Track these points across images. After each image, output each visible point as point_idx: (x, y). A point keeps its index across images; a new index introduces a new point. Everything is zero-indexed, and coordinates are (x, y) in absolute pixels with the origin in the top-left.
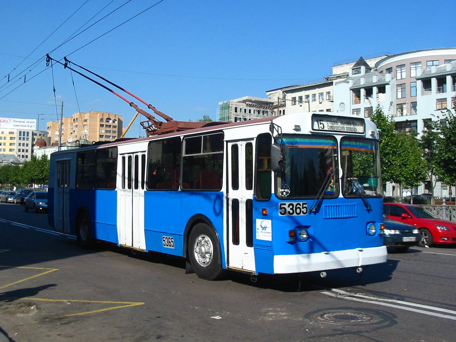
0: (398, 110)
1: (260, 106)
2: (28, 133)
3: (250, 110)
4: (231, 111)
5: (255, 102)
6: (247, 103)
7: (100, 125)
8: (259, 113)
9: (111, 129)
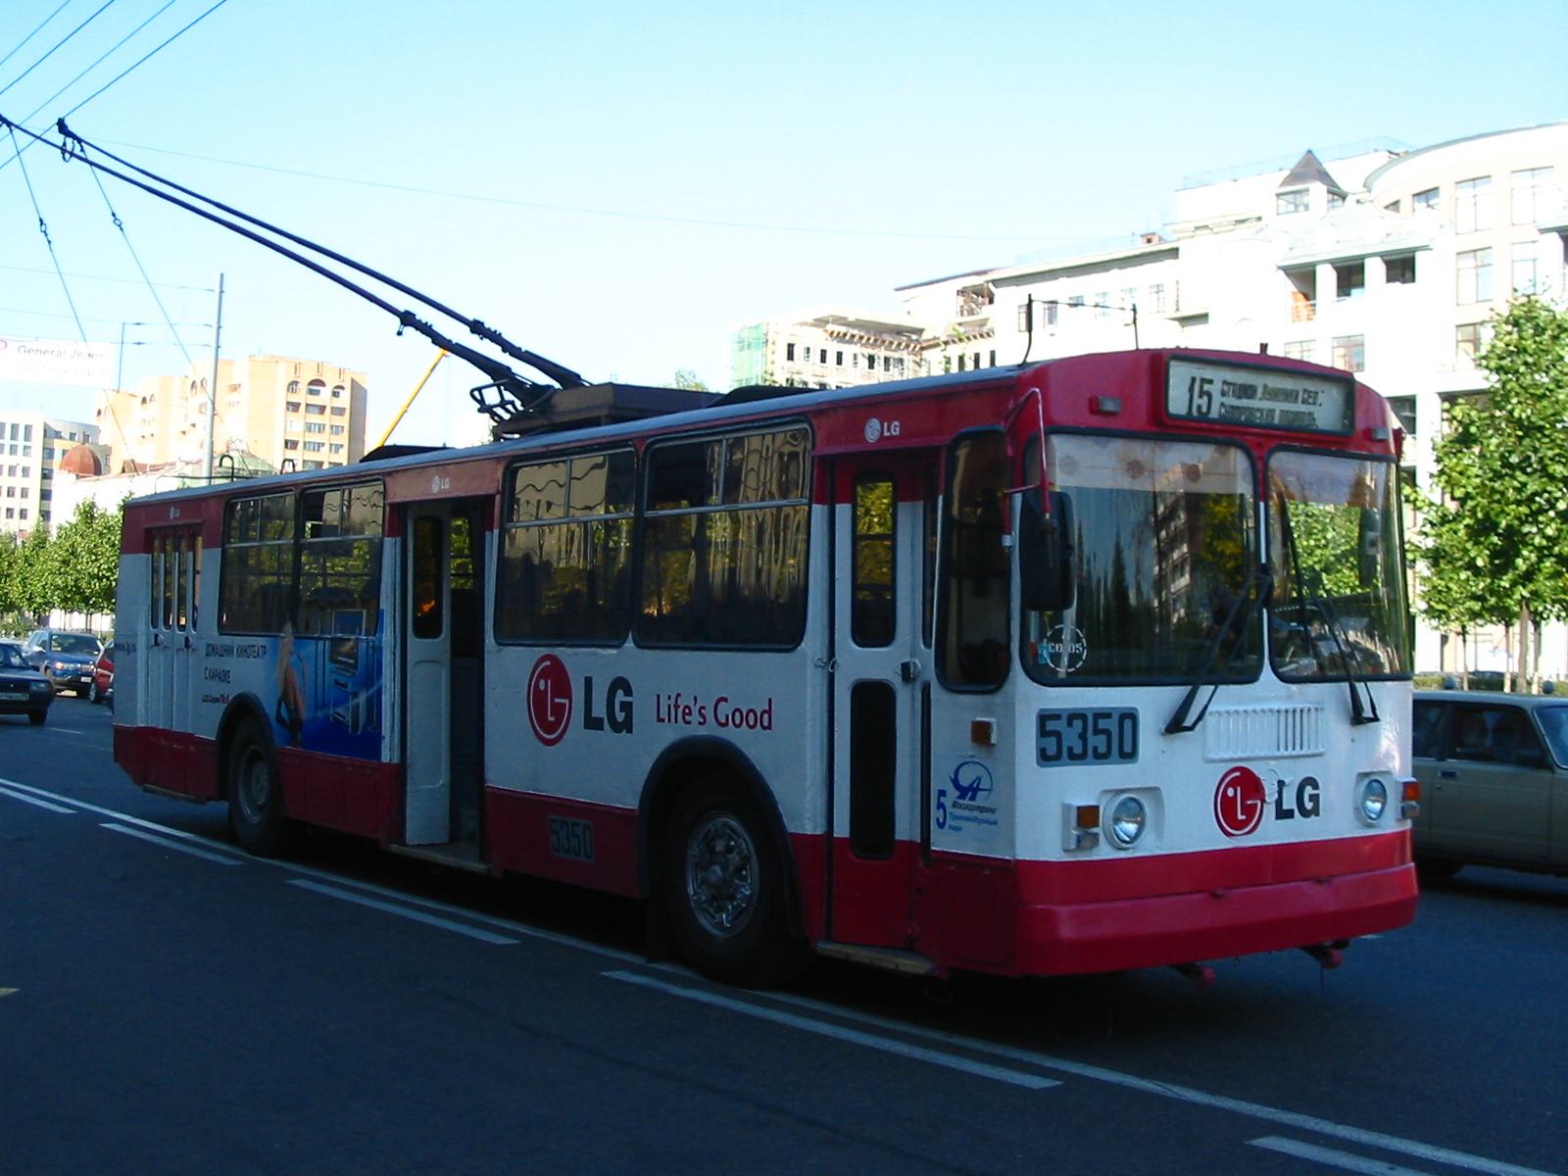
0: (1462, 345)
1: (876, 340)
2: (28, 428)
3: (840, 355)
4: (774, 358)
5: (858, 324)
6: (830, 327)
7: (288, 403)
8: (871, 366)
9: (327, 419)
